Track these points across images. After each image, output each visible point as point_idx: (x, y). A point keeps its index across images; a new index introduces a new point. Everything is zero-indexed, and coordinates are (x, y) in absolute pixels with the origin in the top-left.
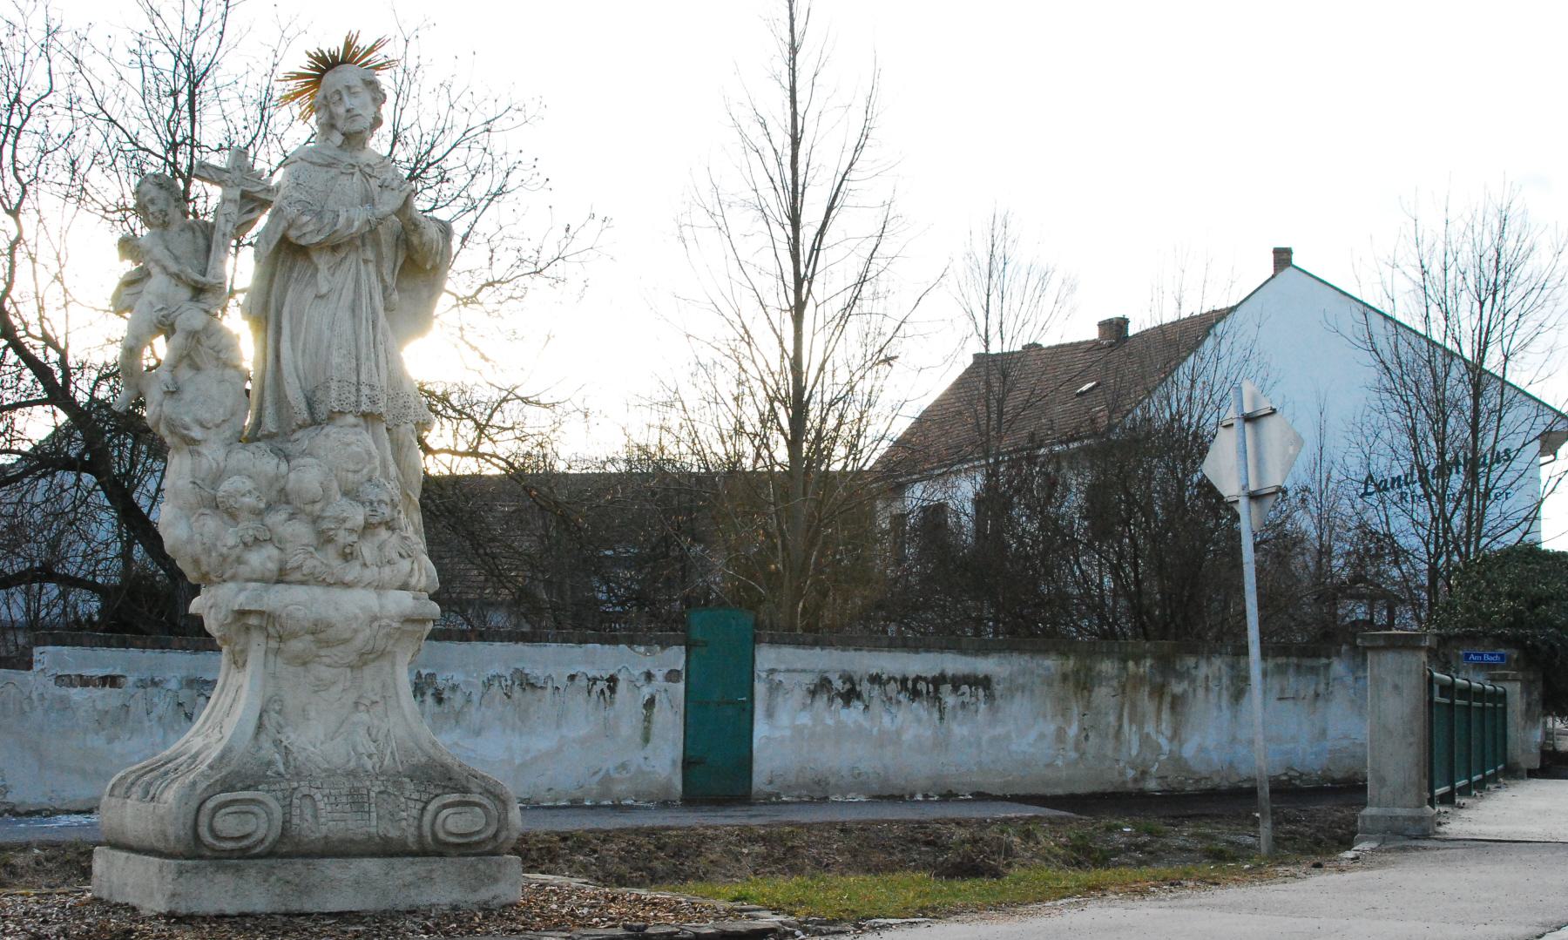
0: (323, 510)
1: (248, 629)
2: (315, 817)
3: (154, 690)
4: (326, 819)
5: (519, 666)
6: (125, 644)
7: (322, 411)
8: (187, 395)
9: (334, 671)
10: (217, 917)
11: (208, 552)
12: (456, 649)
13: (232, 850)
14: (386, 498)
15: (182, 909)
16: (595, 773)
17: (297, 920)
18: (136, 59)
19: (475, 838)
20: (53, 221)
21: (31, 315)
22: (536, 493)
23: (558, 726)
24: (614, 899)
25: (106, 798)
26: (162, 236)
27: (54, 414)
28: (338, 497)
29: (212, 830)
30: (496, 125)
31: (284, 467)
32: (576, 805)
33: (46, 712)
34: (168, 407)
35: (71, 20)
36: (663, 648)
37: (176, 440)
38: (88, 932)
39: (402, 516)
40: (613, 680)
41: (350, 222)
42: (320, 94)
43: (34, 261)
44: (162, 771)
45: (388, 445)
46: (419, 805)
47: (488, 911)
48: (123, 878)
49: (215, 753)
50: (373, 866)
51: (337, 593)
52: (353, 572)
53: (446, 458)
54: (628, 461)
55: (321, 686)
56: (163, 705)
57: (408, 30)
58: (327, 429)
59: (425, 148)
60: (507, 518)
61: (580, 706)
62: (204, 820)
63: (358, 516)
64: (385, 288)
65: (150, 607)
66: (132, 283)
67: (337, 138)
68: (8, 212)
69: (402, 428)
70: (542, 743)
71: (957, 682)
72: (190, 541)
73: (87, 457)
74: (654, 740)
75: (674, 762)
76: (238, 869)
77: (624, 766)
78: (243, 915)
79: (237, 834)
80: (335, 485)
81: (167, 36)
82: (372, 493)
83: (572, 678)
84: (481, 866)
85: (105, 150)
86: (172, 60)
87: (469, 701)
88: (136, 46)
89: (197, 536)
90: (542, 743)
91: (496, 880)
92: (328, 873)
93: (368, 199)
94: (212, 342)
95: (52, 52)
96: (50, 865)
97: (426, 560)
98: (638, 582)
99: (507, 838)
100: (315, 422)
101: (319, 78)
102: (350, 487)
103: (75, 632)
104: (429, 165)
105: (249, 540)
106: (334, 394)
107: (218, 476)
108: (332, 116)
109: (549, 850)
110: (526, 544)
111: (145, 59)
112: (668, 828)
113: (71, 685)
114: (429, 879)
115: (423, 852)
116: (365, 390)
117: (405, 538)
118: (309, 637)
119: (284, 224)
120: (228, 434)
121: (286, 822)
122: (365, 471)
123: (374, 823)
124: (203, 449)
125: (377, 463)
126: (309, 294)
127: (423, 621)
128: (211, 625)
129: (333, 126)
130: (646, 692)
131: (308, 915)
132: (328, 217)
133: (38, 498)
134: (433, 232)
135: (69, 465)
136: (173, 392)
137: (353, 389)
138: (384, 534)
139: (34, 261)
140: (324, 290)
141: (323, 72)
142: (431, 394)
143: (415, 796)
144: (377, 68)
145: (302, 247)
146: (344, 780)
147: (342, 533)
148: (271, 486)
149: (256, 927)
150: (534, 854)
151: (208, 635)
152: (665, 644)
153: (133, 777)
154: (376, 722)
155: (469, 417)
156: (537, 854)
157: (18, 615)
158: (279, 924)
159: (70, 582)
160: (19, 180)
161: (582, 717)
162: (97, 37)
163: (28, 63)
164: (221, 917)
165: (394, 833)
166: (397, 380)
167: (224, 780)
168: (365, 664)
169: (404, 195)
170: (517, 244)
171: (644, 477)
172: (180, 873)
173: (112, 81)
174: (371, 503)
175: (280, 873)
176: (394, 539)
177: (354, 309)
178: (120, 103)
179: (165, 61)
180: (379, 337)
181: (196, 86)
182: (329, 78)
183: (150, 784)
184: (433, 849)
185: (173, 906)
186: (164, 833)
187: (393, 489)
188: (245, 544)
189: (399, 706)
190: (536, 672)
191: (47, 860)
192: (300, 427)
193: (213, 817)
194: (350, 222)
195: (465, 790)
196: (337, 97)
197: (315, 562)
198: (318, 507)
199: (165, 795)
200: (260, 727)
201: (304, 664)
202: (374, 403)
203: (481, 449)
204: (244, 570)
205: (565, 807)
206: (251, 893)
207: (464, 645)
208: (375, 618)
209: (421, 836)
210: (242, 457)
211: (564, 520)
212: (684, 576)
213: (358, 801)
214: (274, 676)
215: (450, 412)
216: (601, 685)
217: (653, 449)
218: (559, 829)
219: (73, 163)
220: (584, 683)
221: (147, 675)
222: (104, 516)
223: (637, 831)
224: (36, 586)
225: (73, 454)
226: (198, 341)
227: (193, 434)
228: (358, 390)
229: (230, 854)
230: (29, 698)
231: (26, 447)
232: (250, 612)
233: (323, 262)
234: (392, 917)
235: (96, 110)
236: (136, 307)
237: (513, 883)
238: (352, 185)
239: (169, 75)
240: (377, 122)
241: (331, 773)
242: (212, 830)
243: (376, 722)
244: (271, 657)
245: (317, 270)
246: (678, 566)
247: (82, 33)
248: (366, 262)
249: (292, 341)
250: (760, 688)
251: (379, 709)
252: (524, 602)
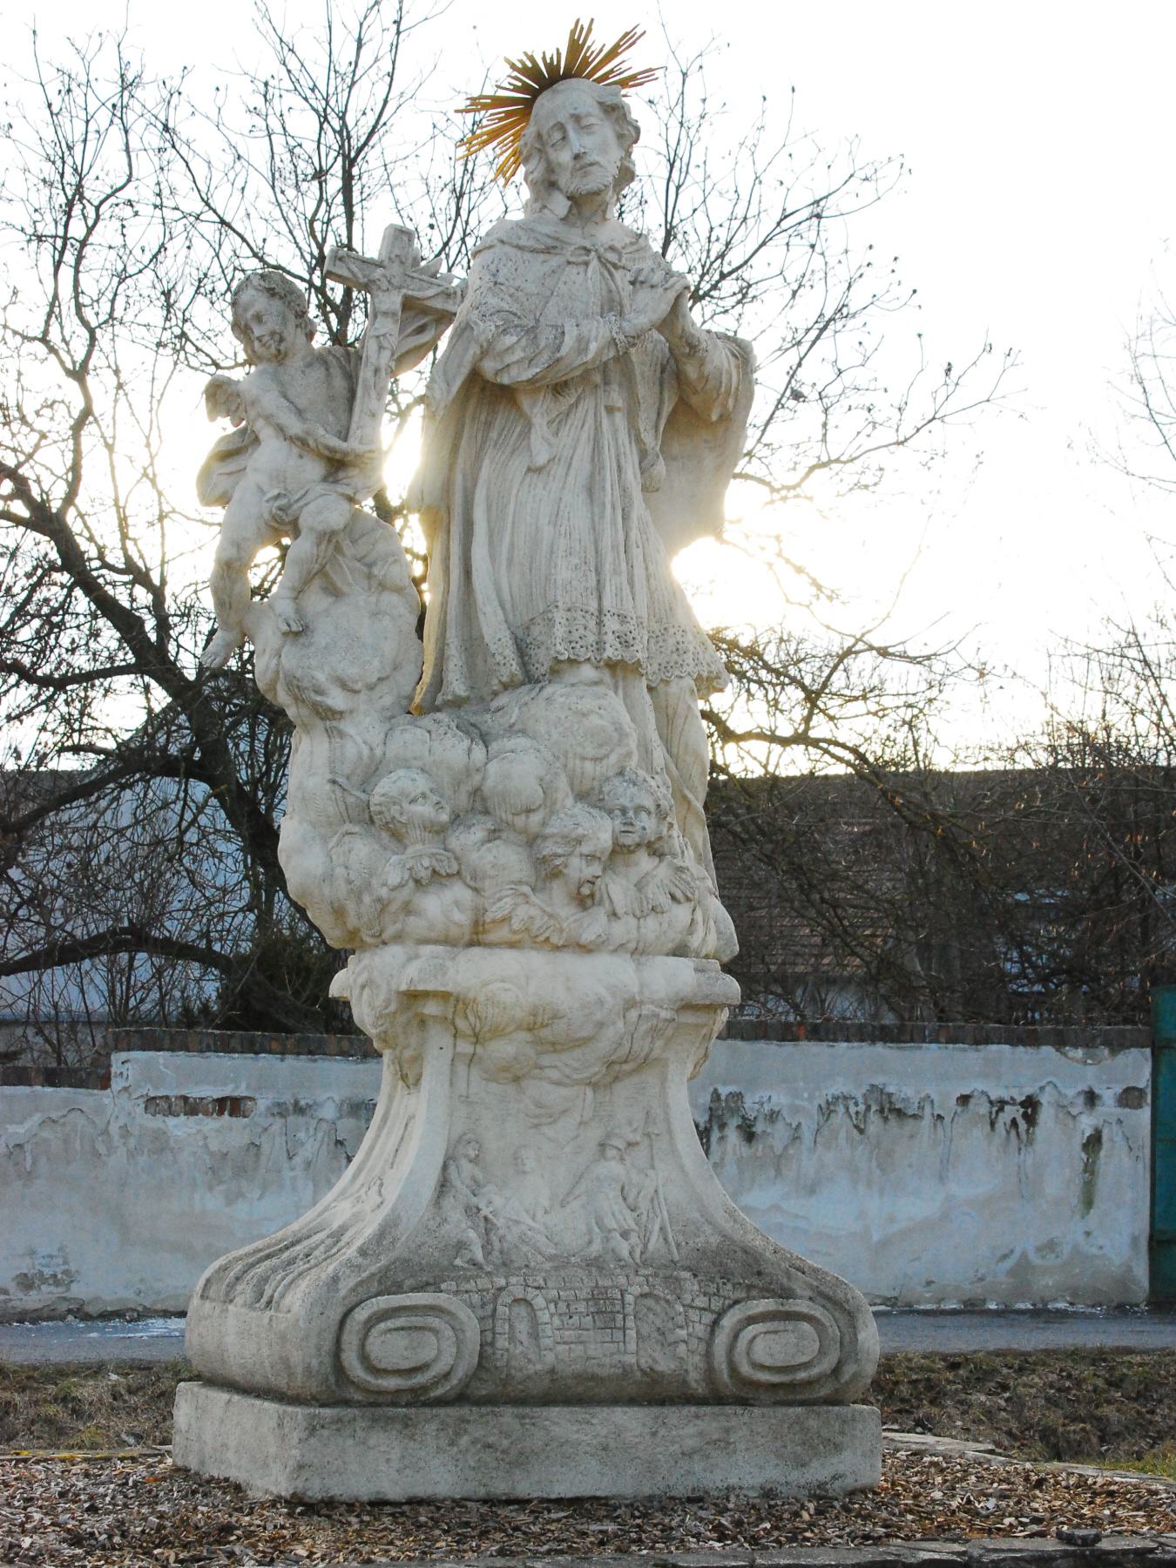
0: (544, 824)
1: (423, 1022)
2: (535, 1335)
3: (301, 1120)
4: (551, 1341)
5: (878, 1080)
6: (253, 1048)
7: (542, 660)
8: (320, 638)
9: (564, 1091)
10: (372, 1504)
11: (358, 895)
12: (772, 1053)
13: (398, 1391)
14: (649, 803)
15: (315, 1491)
16: (1005, 1257)
17: (503, 1512)
18: (261, 124)
19: (802, 1375)
20: (139, 389)
21: (111, 540)
22: (895, 800)
23: (942, 1179)
24: (1040, 1484)
25: (196, 1301)
26: (276, 378)
27: (147, 688)
28: (570, 801)
29: (364, 1358)
30: (830, 207)
31: (479, 753)
32: (972, 1309)
33: (131, 1155)
34: (291, 659)
35: (156, 66)
36: (1114, 1052)
37: (305, 712)
38: (160, 1527)
39: (675, 832)
40: (1031, 1106)
41: (582, 345)
42: (530, 131)
43: (110, 448)
44: (284, 1256)
45: (651, 716)
46: (708, 1318)
47: (823, 1499)
48: (229, 1438)
49: (369, 1230)
50: (631, 1421)
51: (570, 962)
52: (593, 926)
53: (759, 748)
54: (1053, 750)
55: (544, 1116)
56: (312, 1145)
57: (686, 54)
58: (549, 690)
59: (717, 248)
60: (857, 842)
61: (977, 1145)
62: (351, 1339)
63: (602, 832)
64: (643, 454)
65: (282, 995)
66: (232, 453)
67: (560, 205)
68: (71, 373)
69: (674, 688)
70: (916, 1206)
72: (328, 877)
73: (197, 755)
74: (1100, 1205)
75: (1135, 1240)
76: (406, 1423)
77: (1051, 1246)
78: (415, 1502)
79: (406, 1365)
80: (563, 783)
81: (306, 83)
82: (624, 795)
83: (964, 1100)
84: (813, 1423)
85: (215, 270)
86: (314, 121)
87: (796, 1138)
88: (259, 101)
89: (340, 871)
90: (916, 1206)
91: (838, 1448)
92: (556, 1431)
93: (612, 305)
94: (362, 549)
95: (130, 117)
96: (133, 1400)
97: (716, 907)
98: (1068, 943)
99: (855, 1376)
100: (530, 678)
101: (528, 105)
102: (587, 785)
103: (182, 1030)
104: (723, 276)
105: (424, 874)
106: (560, 631)
107: (373, 771)
108: (550, 169)
109: (930, 1385)
110: (886, 883)
111: (275, 124)
112: (1129, 1351)
113: (171, 1112)
114: (724, 1444)
115: (715, 1398)
116: (611, 624)
117: (680, 869)
118: (524, 1036)
119: (474, 350)
120: (388, 700)
121: (486, 1346)
122: (613, 758)
123: (632, 1347)
124: (346, 726)
125: (633, 743)
126: (519, 464)
127: (712, 1008)
128: (363, 1015)
129: (552, 185)
130: (1087, 1124)
131: (522, 1503)
132: (546, 336)
133: (125, 820)
134: (720, 358)
135: (169, 767)
136: (298, 633)
137: (592, 624)
138: (645, 862)
139: (110, 448)
140: (541, 460)
141: (535, 94)
142: (733, 645)
143: (701, 1301)
144: (624, 83)
146: (581, 1273)
147: (575, 862)
148: (457, 784)
149: (436, 1522)
150: (904, 1390)
151: (359, 1032)
152: (1117, 1045)
153: (239, 1267)
154: (635, 1178)
155: (793, 680)
156: (908, 1394)
157: (97, 1002)
158: (474, 1519)
159: (175, 950)
160: (85, 323)
161: (981, 1163)
162: (197, 90)
163: (92, 136)
164: (378, 1504)
165: (665, 1365)
166: (666, 609)
167: (384, 1274)
168: (616, 1079)
169: (672, 295)
170: (867, 399)
171: (1079, 773)
172: (312, 1430)
173: (223, 159)
174: (624, 811)
175: (477, 1431)
176: (663, 871)
177: (591, 490)
178: (238, 194)
179: (304, 125)
180: (634, 534)
181: (352, 162)
182: (544, 102)
183: (265, 1280)
184: (732, 1393)
185: (300, 1485)
186: (285, 1361)
187: (659, 788)
188: (417, 882)
189: (673, 1151)
190: (905, 1091)
191: (130, 1391)
192: (506, 687)
193: (366, 1336)
194: (582, 345)
195: (786, 1294)
196: (557, 136)
197: (533, 912)
198: (536, 818)
199: (287, 1300)
200: (444, 1185)
201: (517, 1079)
202: (626, 644)
203: (813, 734)
204: (415, 925)
205: (954, 1312)
206: (427, 1464)
207: (788, 1047)
208: (630, 1004)
209: (710, 1372)
210: (412, 738)
211: (948, 845)
212: (1145, 935)
213: (605, 1311)
214: (466, 1100)
215: (763, 674)
216: (1011, 1112)
217: (1091, 727)
218: (942, 1349)
219: (167, 294)
220: (984, 1109)
221: (288, 1098)
222: (222, 846)
223: (1075, 1355)
224: (124, 957)
225: (173, 750)
226: (338, 549)
227: (330, 702)
228: (600, 623)
229: (394, 1399)
230: (106, 1132)
231: (110, 744)
232: (426, 995)
233: (539, 412)
234: (663, 1509)
235: (199, 206)
236: (236, 496)
237: (867, 1451)
238: (586, 283)
239: (310, 147)
240: (626, 175)
241: (561, 1262)
242: (364, 1358)
243: (635, 1178)
244: (462, 1069)
245: (529, 425)
246: (1136, 917)
247: (174, 84)
248: (610, 410)
249: (491, 543)
251: (641, 1153)
252: (884, 978)
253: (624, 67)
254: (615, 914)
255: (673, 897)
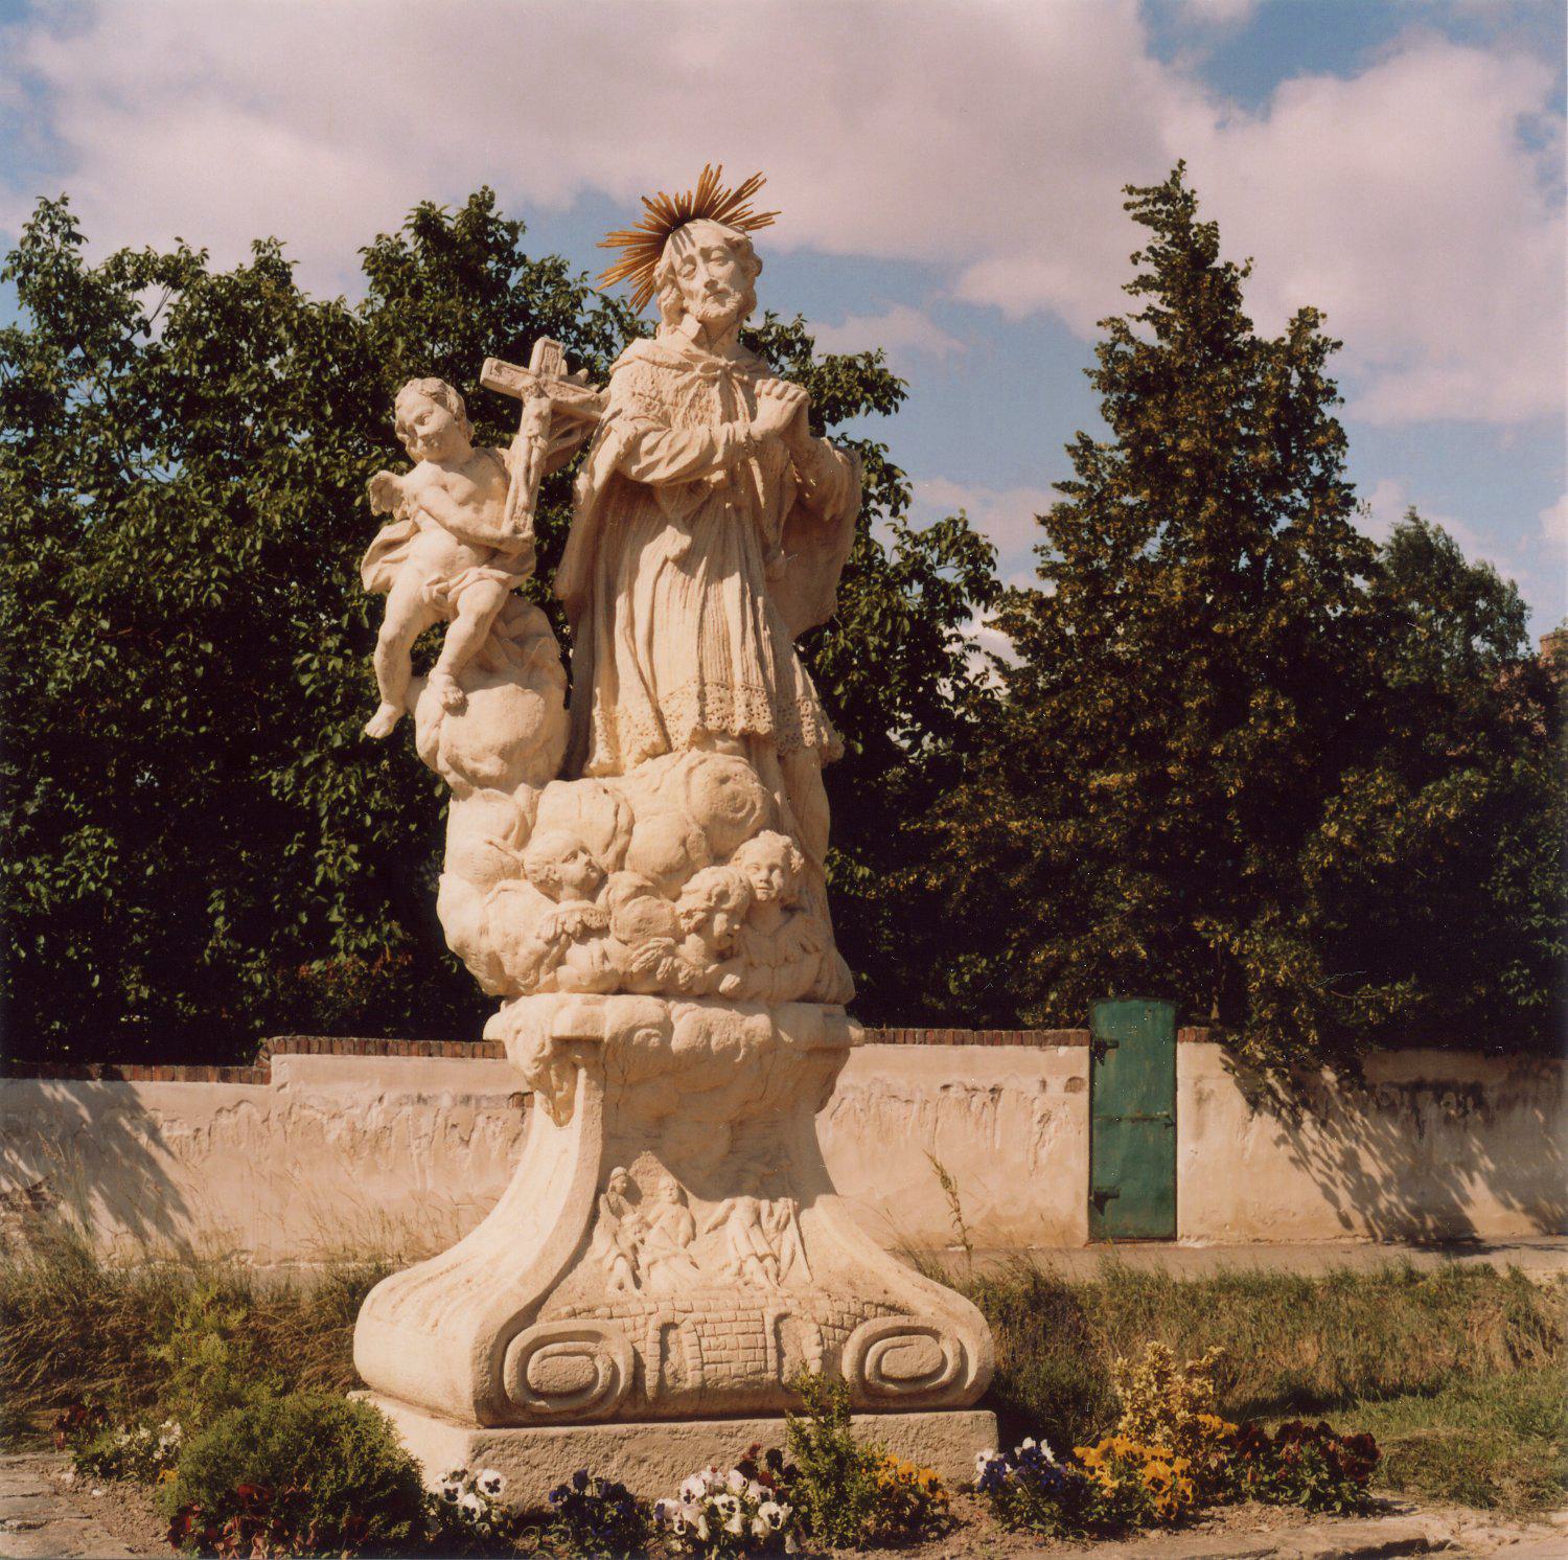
64: (766, 549)
71: (1440, 1089)
83: (946, 1087)
145: (649, 487)
250: (1184, 1098)
253: (747, 210)
254: (751, 964)
255: (805, 949)
